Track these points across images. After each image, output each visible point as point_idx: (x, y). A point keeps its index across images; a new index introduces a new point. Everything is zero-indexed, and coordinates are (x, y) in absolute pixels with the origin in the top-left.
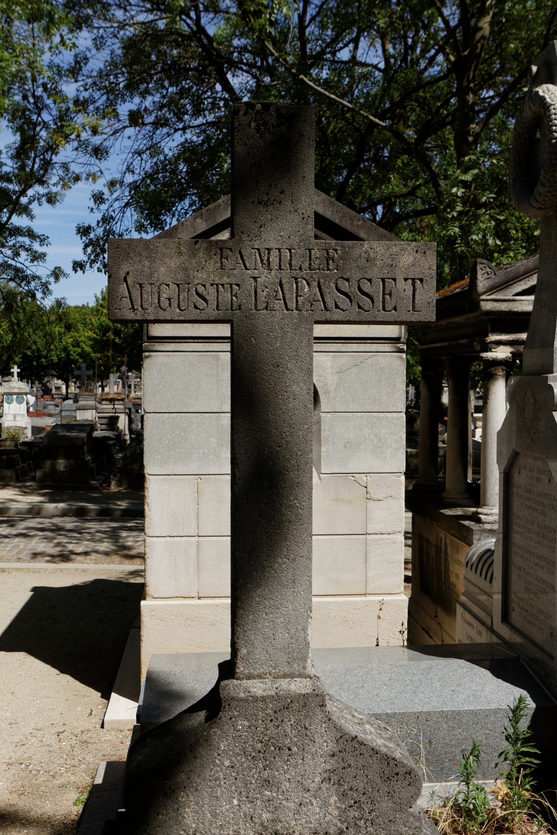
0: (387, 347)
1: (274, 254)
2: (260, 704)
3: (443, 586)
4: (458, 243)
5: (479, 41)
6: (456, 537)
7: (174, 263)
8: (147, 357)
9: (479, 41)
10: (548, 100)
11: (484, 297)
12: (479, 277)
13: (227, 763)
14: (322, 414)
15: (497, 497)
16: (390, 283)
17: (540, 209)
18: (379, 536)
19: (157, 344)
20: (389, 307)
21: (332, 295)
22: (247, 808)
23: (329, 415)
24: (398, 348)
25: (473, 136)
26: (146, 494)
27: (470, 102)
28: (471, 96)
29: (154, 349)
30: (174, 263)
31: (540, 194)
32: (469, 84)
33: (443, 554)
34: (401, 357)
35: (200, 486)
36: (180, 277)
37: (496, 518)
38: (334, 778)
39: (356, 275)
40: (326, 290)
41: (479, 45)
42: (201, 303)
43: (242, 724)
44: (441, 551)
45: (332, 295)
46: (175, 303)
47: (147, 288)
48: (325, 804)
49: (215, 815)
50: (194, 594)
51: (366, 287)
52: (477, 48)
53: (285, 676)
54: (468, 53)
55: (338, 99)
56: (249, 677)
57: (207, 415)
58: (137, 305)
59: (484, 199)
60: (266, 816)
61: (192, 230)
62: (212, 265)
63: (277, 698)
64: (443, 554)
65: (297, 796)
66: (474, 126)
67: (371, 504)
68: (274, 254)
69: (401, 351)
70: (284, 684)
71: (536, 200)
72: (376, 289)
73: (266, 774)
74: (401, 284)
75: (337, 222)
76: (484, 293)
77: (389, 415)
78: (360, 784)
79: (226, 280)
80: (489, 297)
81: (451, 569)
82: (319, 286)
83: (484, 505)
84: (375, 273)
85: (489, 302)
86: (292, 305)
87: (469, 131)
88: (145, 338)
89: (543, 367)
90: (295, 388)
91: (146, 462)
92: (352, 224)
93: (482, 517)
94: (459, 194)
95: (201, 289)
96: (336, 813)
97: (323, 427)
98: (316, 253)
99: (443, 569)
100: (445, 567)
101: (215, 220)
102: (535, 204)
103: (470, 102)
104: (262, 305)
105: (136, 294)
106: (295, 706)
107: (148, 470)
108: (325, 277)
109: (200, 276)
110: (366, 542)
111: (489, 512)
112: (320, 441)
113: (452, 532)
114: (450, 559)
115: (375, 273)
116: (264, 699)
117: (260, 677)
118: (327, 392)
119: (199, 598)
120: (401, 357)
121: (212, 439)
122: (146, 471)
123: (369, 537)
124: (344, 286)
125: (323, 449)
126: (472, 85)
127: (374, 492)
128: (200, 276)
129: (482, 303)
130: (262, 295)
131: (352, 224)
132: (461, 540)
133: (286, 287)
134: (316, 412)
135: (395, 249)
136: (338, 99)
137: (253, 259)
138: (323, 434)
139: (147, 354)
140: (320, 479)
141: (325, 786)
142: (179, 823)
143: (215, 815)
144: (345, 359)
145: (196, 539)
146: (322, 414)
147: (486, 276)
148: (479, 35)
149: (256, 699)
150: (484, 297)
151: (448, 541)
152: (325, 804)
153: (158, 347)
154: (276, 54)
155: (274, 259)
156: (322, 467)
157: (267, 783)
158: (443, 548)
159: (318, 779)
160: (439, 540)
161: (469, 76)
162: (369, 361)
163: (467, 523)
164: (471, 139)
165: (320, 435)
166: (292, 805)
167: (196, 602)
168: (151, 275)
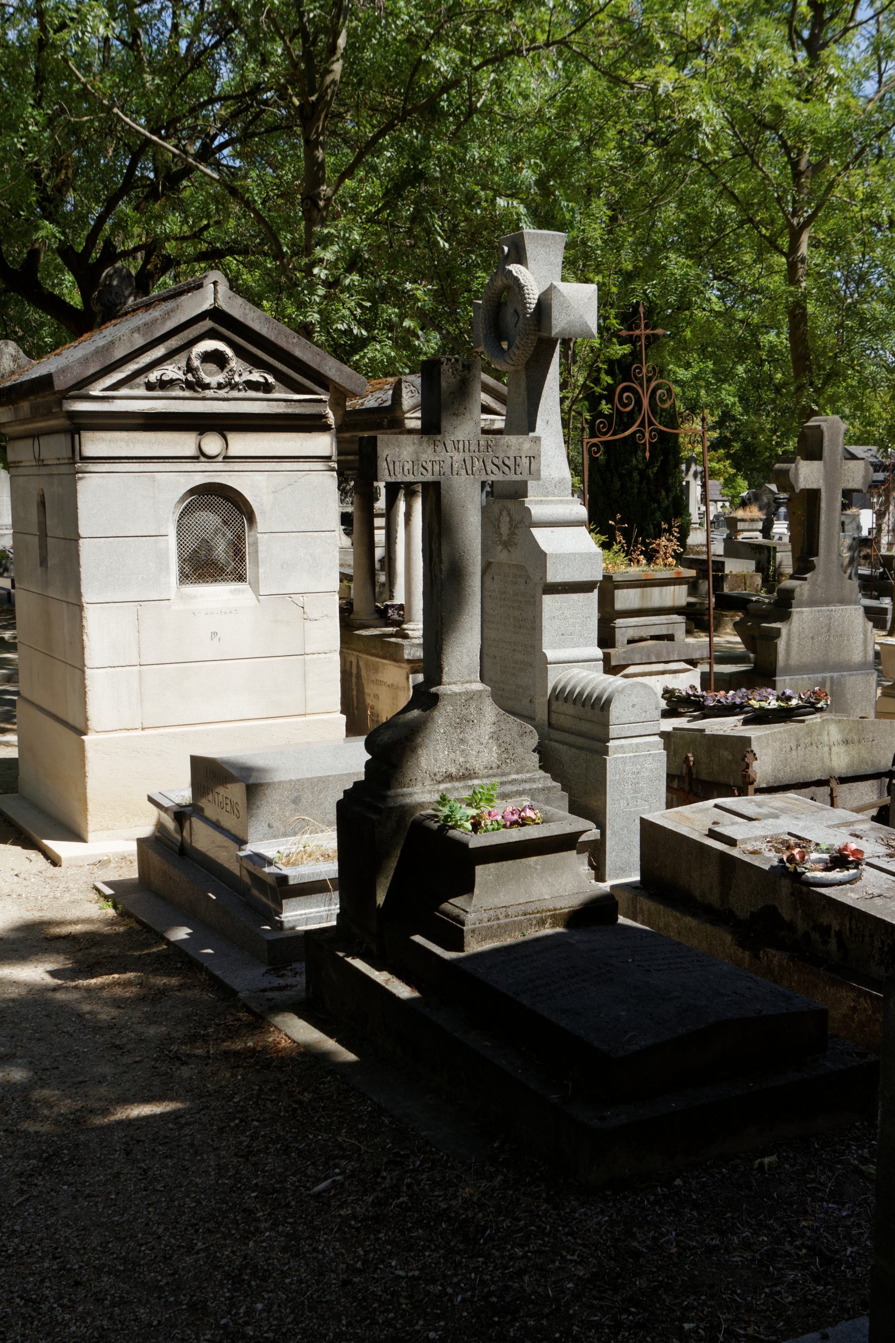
0: (320, 466)
1: (461, 443)
2: (458, 697)
3: (356, 712)
4: (317, 332)
5: (328, 87)
7: (411, 449)
8: (80, 479)
9: (328, 87)
10: (522, 281)
11: (408, 415)
12: (404, 395)
13: (442, 731)
14: (258, 535)
16: (518, 459)
17: (513, 365)
18: (316, 656)
19: (90, 465)
20: (518, 472)
21: (490, 467)
22: (452, 755)
23: (266, 536)
24: (330, 466)
25: (325, 200)
26: (84, 623)
27: (320, 159)
28: (321, 151)
29: (88, 470)
30: (411, 449)
31: (515, 354)
32: (318, 137)
34: (332, 476)
35: (140, 613)
36: (414, 458)
38: (495, 736)
39: (501, 455)
40: (487, 464)
41: (329, 91)
42: (424, 472)
43: (449, 708)
45: (490, 467)
46: (411, 471)
48: (491, 751)
49: (436, 761)
50: (139, 725)
51: (507, 462)
52: (327, 94)
53: (467, 682)
54: (317, 99)
55: (160, 142)
57: (144, 538)
58: (392, 474)
59: (347, 282)
60: (461, 760)
61: (129, 345)
62: (430, 450)
63: (466, 693)
64: (354, 679)
65: (477, 747)
66: (325, 188)
67: (308, 623)
68: (461, 443)
69: (332, 470)
70: (468, 686)
71: (511, 358)
72: (510, 463)
73: (461, 736)
75: (273, 339)
76: (408, 411)
77: (322, 534)
78: (508, 739)
79: (437, 458)
80: (413, 416)
81: (367, 691)
82: (483, 461)
83: (410, 621)
84: (511, 454)
85: (412, 420)
86: (470, 472)
87: (320, 193)
88: (78, 458)
89: (516, 493)
90: (472, 519)
91: (84, 589)
92: (287, 342)
93: (410, 633)
94: (323, 276)
95: (424, 464)
96: (496, 756)
97: (260, 548)
98: (482, 443)
99: (355, 693)
100: (358, 691)
101: (152, 336)
102: (510, 362)
103: (320, 159)
104: (455, 473)
106: (475, 697)
107: (86, 598)
108: (486, 456)
109: (424, 457)
111: (415, 627)
112: (258, 563)
114: (365, 682)
115: (511, 454)
116: (460, 694)
117: (454, 683)
118: (263, 512)
119: (143, 729)
120: (332, 476)
122: (83, 600)
124: (496, 461)
125: (261, 570)
126: (321, 138)
128: (424, 457)
129: (406, 421)
130: (455, 466)
131: (287, 342)
132: (384, 658)
133: (467, 462)
134: (252, 533)
135: (521, 440)
136: (160, 142)
137: (450, 446)
138: (261, 555)
139: (80, 475)
140: (259, 601)
141: (490, 741)
142: (418, 766)
143: (436, 761)
144: (279, 478)
145: (138, 668)
146: (258, 535)
147: (410, 394)
148: (329, 79)
149: (456, 694)
150: (408, 415)
151: (361, 664)
152: (491, 751)
153: (92, 467)
154: (83, 79)
155: (461, 446)
156: (261, 589)
157: (462, 741)
158: (354, 671)
159: (487, 738)
161: (318, 127)
162: (303, 480)
163: (393, 640)
164: (322, 203)
165: (257, 556)
166: (474, 753)
167: (140, 733)
168: (399, 457)
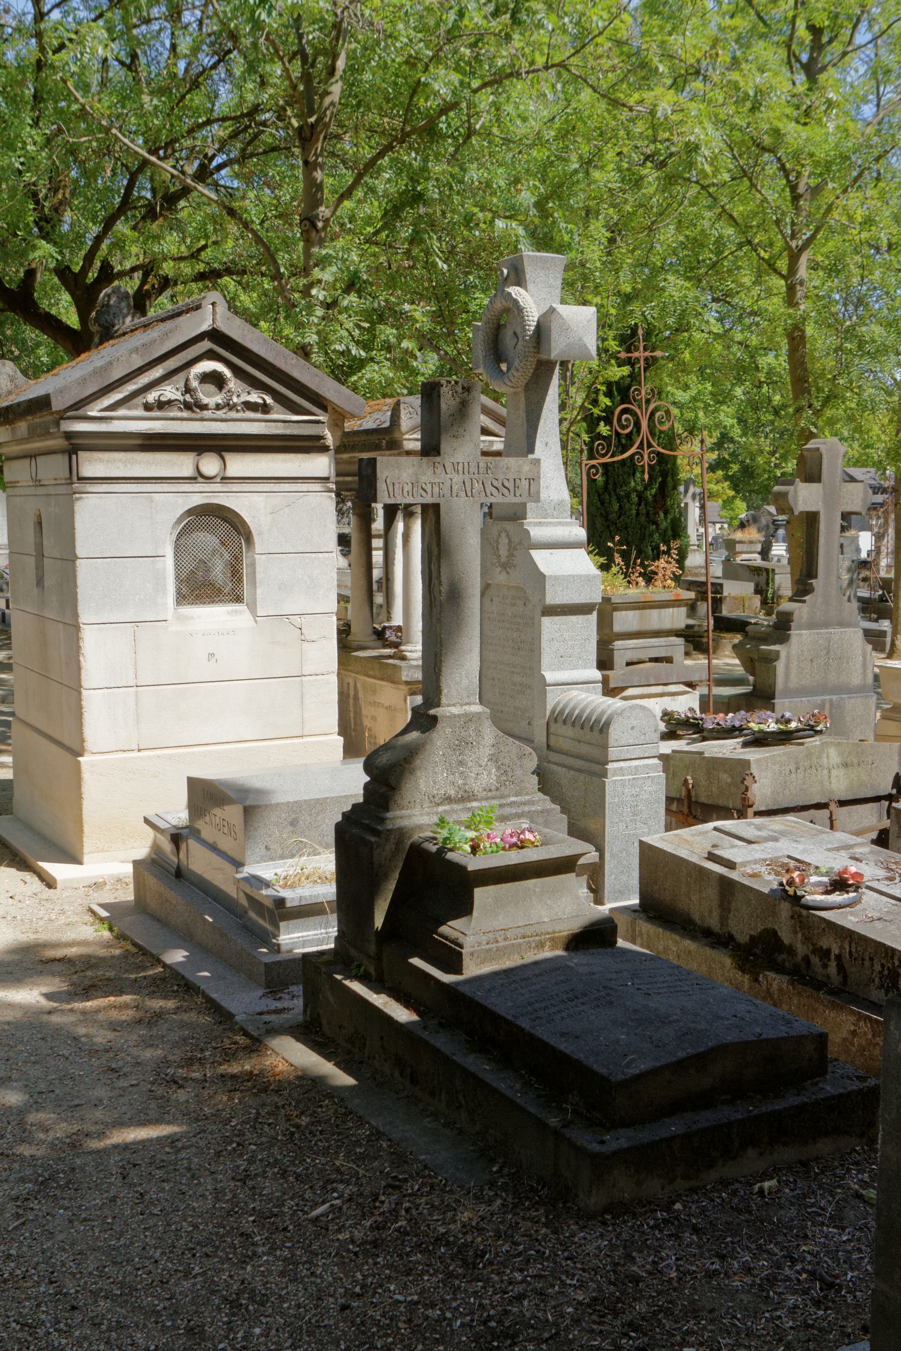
0: (317, 487)
1: (461, 465)
6: (374, 677)
7: (410, 471)
8: (78, 499)
9: (326, 109)
11: (407, 436)
12: (403, 416)
15: (420, 634)
18: (314, 677)
21: (489, 489)
22: (451, 777)
23: (263, 557)
33: (351, 701)
37: (420, 654)
39: (501, 477)
41: (328, 112)
42: (424, 494)
44: (348, 696)
47: (397, 486)
48: (490, 773)
49: (435, 783)
50: (135, 747)
51: (506, 484)
56: (448, 706)
60: (460, 782)
63: (465, 715)
64: (351, 701)
65: (475, 770)
67: (306, 645)
68: (461, 465)
69: (330, 491)
70: (467, 708)
72: (510, 485)
74: (523, 481)
78: (507, 761)
79: (437, 480)
84: (511, 476)
86: (469, 494)
90: (471, 541)
91: (80, 610)
93: (408, 654)
97: (258, 569)
98: (482, 465)
99: (352, 715)
100: (355, 713)
104: (454, 494)
105: (391, 489)
109: (424, 479)
110: (302, 684)
112: (255, 584)
113: (371, 673)
114: (362, 704)
116: (459, 716)
118: (260, 533)
121: (148, 585)
123: (304, 678)
124: (495, 483)
125: (259, 591)
127: (308, 633)
129: (405, 443)
130: (455, 488)
134: (250, 554)
137: (449, 468)
138: (258, 576)
144: (277, 499)
149: (455, 716)
150: (407, 436)
151: (359, 685)
152: (490, 773)
155: (460, 468)
157: (461, 763)
158: (352, 693)
160: (345, 685)
162: (301, 501)
163: (391, 661)
167: (136, 754)
